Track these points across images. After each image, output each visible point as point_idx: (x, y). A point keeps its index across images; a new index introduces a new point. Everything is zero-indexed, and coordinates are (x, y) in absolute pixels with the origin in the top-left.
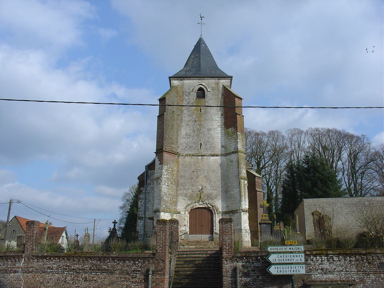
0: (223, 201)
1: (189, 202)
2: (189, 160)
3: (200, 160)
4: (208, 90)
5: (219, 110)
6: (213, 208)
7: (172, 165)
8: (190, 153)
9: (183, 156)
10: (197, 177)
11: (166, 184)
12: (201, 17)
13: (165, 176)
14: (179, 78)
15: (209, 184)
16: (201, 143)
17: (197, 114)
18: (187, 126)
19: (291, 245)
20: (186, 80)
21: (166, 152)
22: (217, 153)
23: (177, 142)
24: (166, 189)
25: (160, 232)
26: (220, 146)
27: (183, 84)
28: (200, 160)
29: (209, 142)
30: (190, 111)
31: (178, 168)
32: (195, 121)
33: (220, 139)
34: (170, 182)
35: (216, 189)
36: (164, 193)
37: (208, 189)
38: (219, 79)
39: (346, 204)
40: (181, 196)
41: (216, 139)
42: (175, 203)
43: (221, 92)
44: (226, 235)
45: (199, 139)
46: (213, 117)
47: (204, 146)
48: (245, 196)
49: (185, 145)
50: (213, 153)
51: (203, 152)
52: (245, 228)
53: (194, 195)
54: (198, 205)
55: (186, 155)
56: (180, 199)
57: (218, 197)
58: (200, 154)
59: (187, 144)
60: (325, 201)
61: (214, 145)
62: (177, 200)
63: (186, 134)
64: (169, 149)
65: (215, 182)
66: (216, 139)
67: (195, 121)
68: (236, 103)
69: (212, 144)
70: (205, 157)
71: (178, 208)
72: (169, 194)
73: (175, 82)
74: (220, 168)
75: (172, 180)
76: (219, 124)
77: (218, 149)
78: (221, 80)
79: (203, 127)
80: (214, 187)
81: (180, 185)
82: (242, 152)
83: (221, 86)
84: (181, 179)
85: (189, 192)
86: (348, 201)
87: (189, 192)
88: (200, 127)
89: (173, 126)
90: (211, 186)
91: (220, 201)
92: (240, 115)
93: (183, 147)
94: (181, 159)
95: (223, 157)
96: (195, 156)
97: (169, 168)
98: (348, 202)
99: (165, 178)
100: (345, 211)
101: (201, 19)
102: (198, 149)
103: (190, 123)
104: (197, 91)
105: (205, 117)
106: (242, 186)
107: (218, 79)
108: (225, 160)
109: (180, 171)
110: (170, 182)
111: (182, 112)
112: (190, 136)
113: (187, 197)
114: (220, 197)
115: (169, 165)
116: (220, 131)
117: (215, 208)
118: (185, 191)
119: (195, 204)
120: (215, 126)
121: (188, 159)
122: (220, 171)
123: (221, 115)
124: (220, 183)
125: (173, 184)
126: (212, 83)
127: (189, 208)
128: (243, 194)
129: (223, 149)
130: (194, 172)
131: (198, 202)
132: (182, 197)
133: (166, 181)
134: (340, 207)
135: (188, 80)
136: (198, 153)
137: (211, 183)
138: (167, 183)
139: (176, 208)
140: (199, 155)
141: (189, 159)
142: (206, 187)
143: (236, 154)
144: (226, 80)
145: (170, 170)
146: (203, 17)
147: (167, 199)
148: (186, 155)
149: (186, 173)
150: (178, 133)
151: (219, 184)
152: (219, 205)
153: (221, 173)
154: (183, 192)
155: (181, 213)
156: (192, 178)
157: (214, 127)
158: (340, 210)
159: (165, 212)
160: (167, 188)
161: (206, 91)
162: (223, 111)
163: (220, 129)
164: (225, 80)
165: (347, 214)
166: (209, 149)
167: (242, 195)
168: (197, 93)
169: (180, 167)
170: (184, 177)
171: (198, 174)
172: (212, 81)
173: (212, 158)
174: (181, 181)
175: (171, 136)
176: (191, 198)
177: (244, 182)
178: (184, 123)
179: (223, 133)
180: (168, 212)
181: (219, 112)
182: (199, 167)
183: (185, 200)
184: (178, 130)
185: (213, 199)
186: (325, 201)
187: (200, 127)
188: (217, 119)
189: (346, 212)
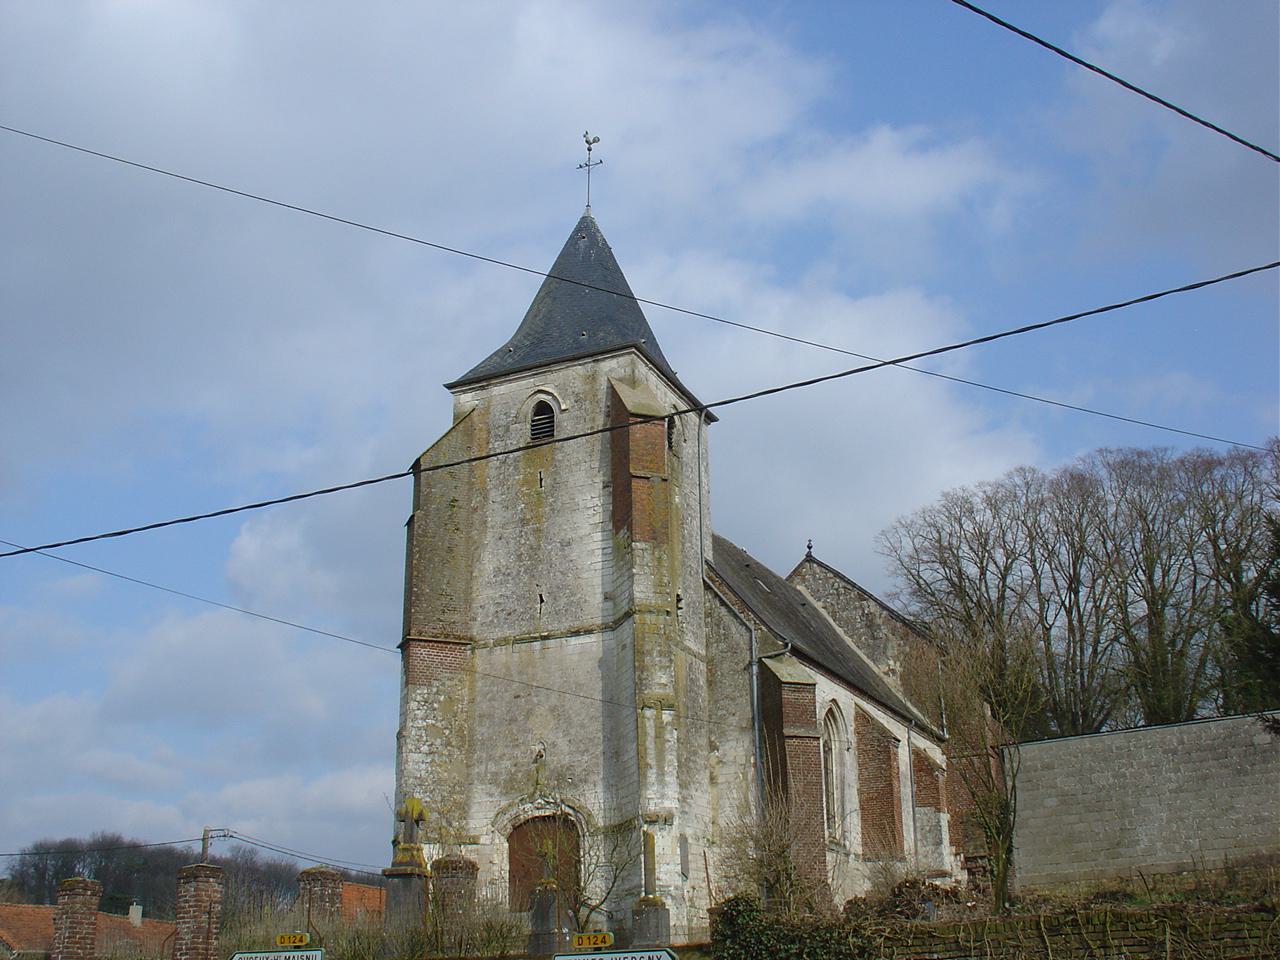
0: (608, 787)
1: (504, 803)
2: (504, 658)
3: (537, 655)
4: (563, 407)
5: (596, 471)
6: (576, 816)
7: (448, 683)
8: (508, 633)
9: (485, 646)
10: (529, 713)
11: (425, 749)
12: (587, 142)
13: (421, 723)
14: (477, 382)
15: (566, 733)
16: (541, 596)
17: (529, 495)
18: (500, 543)
19: (298, 947)
20: (495, 385)
21: (422, 644)
22: (590, 622)
23: (468, 601)
24: (424, 766)
25: (61, 918)
26: (599, 598)
27: (489, 400)
28: (537, 655)
29: (567, 587)
30: (508, 489)
31: (472, 688)
32: (524, 522)
33: (599, 573)
34: (439, 740)
35: (587, 751)
36: (416, 778)
37: (562, 754)
38: (598, 360)
39: (1175, 752)
40: (482, 782)
41: (585, 575)
42: (464, 809)
43: (602, 405)
44: (184, 918)
45: (536, 582)
46: (579, 499)
47: (551, 601)
48: (661, 768)
49: (492, 609)
50: (577, 624)
51: (547, 625)
53: (520, 775)
54: (530, 810)
55: (498, 643)
56: (476, 795)
57: (593, 778)
58: (537, 635)
59: (500, 604)
60: (1088, 746)
61: (579, 596)
62: (468, 798)
63: (497, 571)
65: (583, 726)
66: (585, 575)
67: (524, 522)
68: (631, 437)
69: (573, 595)
70: (551, 643)
71: (472, 824)
72: (438, 782)
73: (468, 399)
74: (598, 673)
75: (447, 732)
76: (598, 519)
77: (595, 609)
78: (602, 364)
79: (547, 538)
80: (581, 741)
81: (478, 747)
82: (650, 612)
83: (603, 385)
84: (480, 724)
85: (503, 766)
86: (1182, 738)
87: (503, 766)
88: (538, 539)
89: (450, 549)
90: (570, 741)
91: (600, 789)
92: (648, 478)
93: (488, 616)
94: (480, 660)
95: (609, 635)
96: (522, 641)
97: (437, 693)
98: (1183, 743)
100: (1170, 780)
101: (589, 150)
102: (530, 618)
103: (508, 532)
104: (535, 415)
105: (554, 502)
106: (646, 734)
108: (613, 644)
109: (479, 699)
110: (439, 740)
111: (486, 498)
112: (509, 574)
113: (498, 786)
114: (598, 777)
115: (436, 683)
116: (600, 545)
117: (581, 817)
118: (492, 767)
119: (521, 808)
120: (585, 530)
121: (501, 655)
122: (599, 685)
123: (604, 487)
124: (598, 725)
125: (453, 746)
126: (574, 379)
127: (505, 820)
128: (651, 760)
129: (609, 604)
130: (518, 696)
131: (532, 798)
132: (484, 787)
133: (425, 739)
134: (1147, 765)
135: (501, 383)
136: (531, 629)
137: (573, 731)
138: (429, 743)
139: (467, 824)
140: (532, 638)
141: (506, 654)
142: (554, 745)
143: (631, 620)
144: (620, 359)
145: (442, 698)
146: (596, 140)
147: (428, 800)
148: (498, 643)
149: (496, 704)
150: (472, 573)
151: (595, 729)
152: (595, 802)
153: (604, 692)
154: (486, 767)
155: (482, 841)
156: (513, 720)
157: (582, 532)
158: (1147, 777)
160: (429, 760)
161: (558, 411)
162: (609, 473)
163: (598, 536)
164: (615, 361)
165: (1179, 790)
166: (566, 611)
167: (647, 764)
168: (533, 421)
169: (480, 684)
170: (490, 716)
171: (533, 702)
172: (576, 373)
173: (574, 641)
174: (482, 731)
175: (444, 587)
176: (509, 786)
177: (658, 718)
178: (489, 535)
179: (609, 551)
181: (596, 476)
182: (533, 680)
183: (491, 795)
184: (472, 560)
185: (576, 786)
186: (1088, 746)
187: (538, 539)
188: (590, 505)
189: (1173, 786)
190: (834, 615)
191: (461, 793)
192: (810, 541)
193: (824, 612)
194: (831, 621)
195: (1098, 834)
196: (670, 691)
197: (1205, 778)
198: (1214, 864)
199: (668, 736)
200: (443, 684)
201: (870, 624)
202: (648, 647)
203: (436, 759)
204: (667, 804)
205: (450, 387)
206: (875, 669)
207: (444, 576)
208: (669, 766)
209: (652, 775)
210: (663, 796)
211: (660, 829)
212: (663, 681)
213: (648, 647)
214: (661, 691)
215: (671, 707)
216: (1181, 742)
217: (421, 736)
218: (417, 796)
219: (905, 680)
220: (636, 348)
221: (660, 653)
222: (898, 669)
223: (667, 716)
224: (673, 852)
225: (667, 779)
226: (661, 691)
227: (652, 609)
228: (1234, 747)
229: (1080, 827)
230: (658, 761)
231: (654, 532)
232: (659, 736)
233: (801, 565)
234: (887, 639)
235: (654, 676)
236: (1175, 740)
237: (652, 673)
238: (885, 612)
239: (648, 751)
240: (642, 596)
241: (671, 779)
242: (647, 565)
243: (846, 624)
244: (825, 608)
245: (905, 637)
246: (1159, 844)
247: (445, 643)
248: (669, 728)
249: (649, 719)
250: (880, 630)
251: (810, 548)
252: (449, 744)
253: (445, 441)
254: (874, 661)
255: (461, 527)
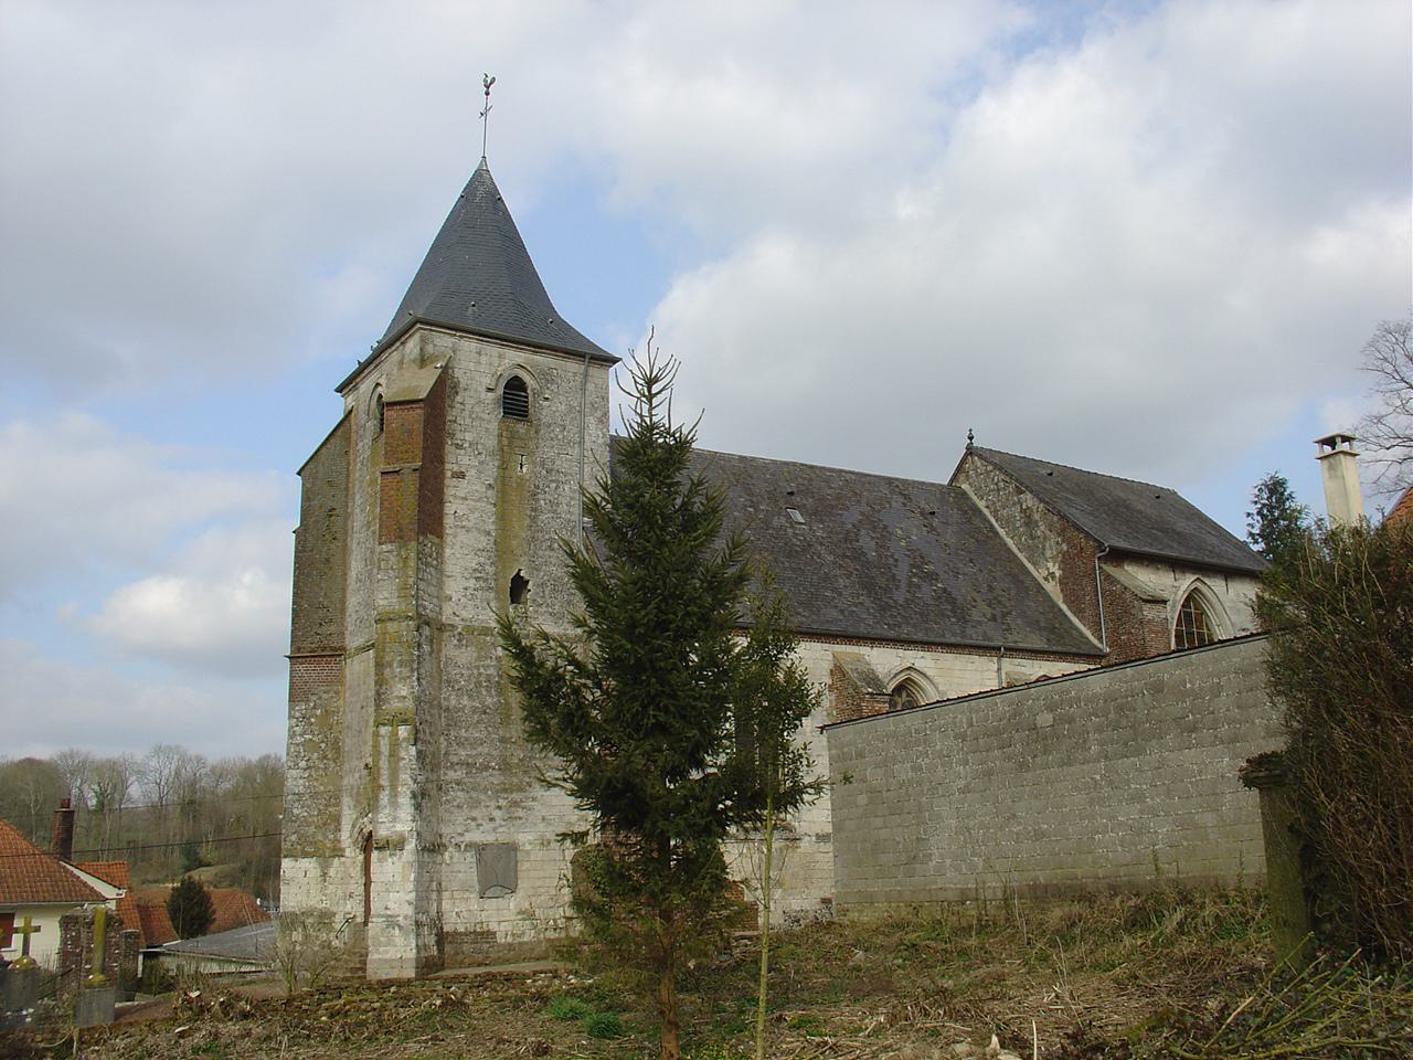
7: (325, 696)
11: (303, 764)
24: (301, 781)
34: (316, 754)
36: (294, 794)
48: (393, 787)
52: (386, 908)
60: (892, 728)
64: (313, 646)
72: (315, 795)
75: (323, 745)
97: (314, 708)
99: (298, 745)
107: (402, 343)
110: (316, 754)
115: (314, 698)
128: (384, 781)
134: (941, 756)
147: (305, 814)
159: (295, 857)
165: (966, 790)
175: (321, 599)
180: (306, 855)
186: (892, 728)
189: (962, 783)
190: (995, 513)
191: (334, 805)
192: (971, 430)
193: (986, 511)
194: (993, 521)
195: (898, 843)
196: (410, 704)
197: (989, 773)
198: (994, 893)
199: (403, 754)
200: (320, 698)
201: (1029, 522)
202: (388, 658)
203: (313, 773)
204: (399, 827)
205: (339, 390)
206: (1035, 573)
207: (322, 589)
208: (403, 785)
209: (384, 797)
210: (395, 819)
211: (391, 855)
212: (404, 693)
213: (388, 658)
214: (400, 705)
215: (405, 722)
216: (971, 725)
217: (299, 752)
218: (296, 811)
219: (1063, 583)
220: (421, 323)
221: (401, 664)
222: (1058, 573)
223: (403, 731)
224: (405, 878)
225: (400, 800)
226: (400, 705)
227: (391, 616)
228: (1017, 730)
229: (884, 833)
230: (391, 781)
231: (401, 531)
232: (394, 755)
233: (963, 461)
234: (1045, 538)
235: (394, 689)
236: (964, 721)
237: (391, 687)
238: (1042, 505)
239: (382, 771)
240: (385, 602)
241: (405, 801)
242: (392, 568)
243: (1007, 523)
244: (987, 507)
245: (1061, 533)
246: (948, 861)
247: (320, 656)
248: (404, 745)
249: (383, 736)
250: (1037, 526)
251: (971, 438)
252: (325, 757)
253: (323, 450)
254: (1034, 564)
255: (338, 535)
